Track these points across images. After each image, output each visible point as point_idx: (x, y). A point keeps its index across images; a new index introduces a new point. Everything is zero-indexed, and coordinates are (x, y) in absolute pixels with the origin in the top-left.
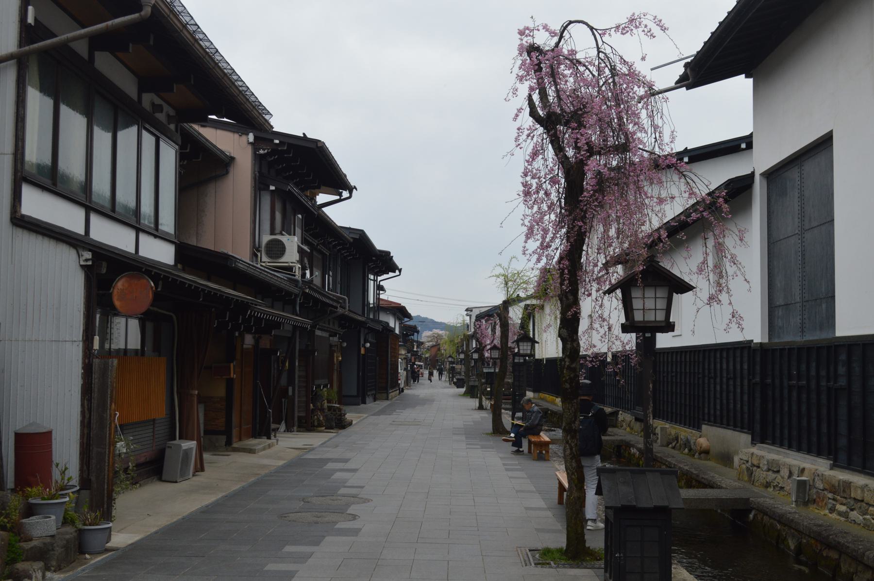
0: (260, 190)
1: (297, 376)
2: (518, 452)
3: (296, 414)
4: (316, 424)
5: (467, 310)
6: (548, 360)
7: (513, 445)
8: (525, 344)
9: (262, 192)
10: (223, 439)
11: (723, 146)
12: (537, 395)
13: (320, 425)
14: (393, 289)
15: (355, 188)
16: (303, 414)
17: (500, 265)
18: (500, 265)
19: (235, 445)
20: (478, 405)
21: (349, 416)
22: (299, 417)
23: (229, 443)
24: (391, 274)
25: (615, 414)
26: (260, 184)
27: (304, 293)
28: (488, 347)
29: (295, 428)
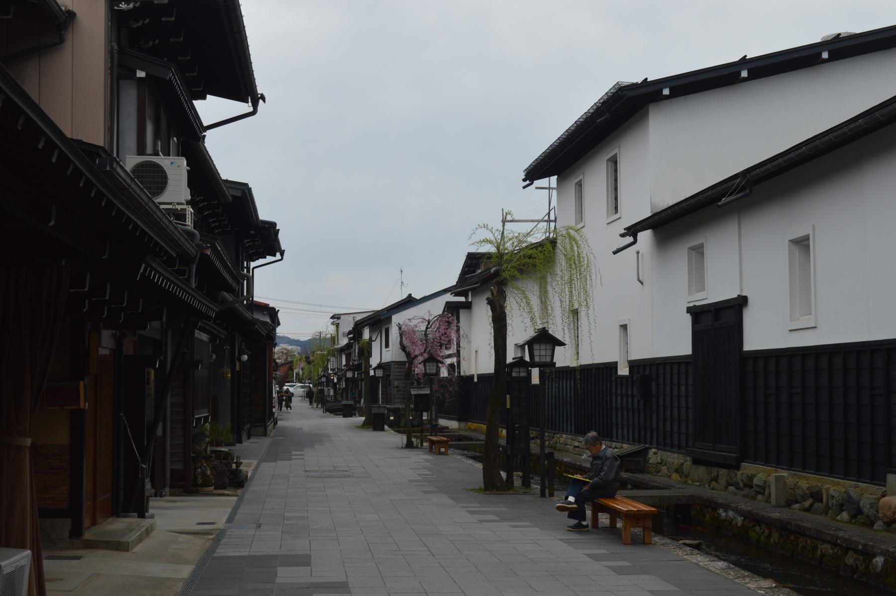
0: (119, 78)
1: (169, 405)
2: (579, 528)
3: (169, 467)
4: (200, 481)
5: (333, 317)
6: (481, 377)
7: (570, 516)
8: (543, 347)
9: (122, 82)
10: (64, 526)
11: (796, 55)
12: (463, 425)
13: (206, 484)
14: (267, 282)
15: (263, 98)
16: (179, 466)
17: (485, 226)
18: (485, 226)
19: (88, 535)
20: (405, 442)
21: (248, 466)
22: (173, 472)
23: (76, 532)
24: (269, 259)
25: (643, 453)
26: (119, 70)
27: (204, 256)
28: (420, 359)
29: (167, 489)
